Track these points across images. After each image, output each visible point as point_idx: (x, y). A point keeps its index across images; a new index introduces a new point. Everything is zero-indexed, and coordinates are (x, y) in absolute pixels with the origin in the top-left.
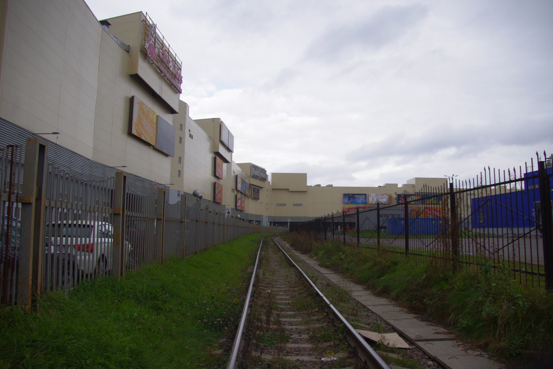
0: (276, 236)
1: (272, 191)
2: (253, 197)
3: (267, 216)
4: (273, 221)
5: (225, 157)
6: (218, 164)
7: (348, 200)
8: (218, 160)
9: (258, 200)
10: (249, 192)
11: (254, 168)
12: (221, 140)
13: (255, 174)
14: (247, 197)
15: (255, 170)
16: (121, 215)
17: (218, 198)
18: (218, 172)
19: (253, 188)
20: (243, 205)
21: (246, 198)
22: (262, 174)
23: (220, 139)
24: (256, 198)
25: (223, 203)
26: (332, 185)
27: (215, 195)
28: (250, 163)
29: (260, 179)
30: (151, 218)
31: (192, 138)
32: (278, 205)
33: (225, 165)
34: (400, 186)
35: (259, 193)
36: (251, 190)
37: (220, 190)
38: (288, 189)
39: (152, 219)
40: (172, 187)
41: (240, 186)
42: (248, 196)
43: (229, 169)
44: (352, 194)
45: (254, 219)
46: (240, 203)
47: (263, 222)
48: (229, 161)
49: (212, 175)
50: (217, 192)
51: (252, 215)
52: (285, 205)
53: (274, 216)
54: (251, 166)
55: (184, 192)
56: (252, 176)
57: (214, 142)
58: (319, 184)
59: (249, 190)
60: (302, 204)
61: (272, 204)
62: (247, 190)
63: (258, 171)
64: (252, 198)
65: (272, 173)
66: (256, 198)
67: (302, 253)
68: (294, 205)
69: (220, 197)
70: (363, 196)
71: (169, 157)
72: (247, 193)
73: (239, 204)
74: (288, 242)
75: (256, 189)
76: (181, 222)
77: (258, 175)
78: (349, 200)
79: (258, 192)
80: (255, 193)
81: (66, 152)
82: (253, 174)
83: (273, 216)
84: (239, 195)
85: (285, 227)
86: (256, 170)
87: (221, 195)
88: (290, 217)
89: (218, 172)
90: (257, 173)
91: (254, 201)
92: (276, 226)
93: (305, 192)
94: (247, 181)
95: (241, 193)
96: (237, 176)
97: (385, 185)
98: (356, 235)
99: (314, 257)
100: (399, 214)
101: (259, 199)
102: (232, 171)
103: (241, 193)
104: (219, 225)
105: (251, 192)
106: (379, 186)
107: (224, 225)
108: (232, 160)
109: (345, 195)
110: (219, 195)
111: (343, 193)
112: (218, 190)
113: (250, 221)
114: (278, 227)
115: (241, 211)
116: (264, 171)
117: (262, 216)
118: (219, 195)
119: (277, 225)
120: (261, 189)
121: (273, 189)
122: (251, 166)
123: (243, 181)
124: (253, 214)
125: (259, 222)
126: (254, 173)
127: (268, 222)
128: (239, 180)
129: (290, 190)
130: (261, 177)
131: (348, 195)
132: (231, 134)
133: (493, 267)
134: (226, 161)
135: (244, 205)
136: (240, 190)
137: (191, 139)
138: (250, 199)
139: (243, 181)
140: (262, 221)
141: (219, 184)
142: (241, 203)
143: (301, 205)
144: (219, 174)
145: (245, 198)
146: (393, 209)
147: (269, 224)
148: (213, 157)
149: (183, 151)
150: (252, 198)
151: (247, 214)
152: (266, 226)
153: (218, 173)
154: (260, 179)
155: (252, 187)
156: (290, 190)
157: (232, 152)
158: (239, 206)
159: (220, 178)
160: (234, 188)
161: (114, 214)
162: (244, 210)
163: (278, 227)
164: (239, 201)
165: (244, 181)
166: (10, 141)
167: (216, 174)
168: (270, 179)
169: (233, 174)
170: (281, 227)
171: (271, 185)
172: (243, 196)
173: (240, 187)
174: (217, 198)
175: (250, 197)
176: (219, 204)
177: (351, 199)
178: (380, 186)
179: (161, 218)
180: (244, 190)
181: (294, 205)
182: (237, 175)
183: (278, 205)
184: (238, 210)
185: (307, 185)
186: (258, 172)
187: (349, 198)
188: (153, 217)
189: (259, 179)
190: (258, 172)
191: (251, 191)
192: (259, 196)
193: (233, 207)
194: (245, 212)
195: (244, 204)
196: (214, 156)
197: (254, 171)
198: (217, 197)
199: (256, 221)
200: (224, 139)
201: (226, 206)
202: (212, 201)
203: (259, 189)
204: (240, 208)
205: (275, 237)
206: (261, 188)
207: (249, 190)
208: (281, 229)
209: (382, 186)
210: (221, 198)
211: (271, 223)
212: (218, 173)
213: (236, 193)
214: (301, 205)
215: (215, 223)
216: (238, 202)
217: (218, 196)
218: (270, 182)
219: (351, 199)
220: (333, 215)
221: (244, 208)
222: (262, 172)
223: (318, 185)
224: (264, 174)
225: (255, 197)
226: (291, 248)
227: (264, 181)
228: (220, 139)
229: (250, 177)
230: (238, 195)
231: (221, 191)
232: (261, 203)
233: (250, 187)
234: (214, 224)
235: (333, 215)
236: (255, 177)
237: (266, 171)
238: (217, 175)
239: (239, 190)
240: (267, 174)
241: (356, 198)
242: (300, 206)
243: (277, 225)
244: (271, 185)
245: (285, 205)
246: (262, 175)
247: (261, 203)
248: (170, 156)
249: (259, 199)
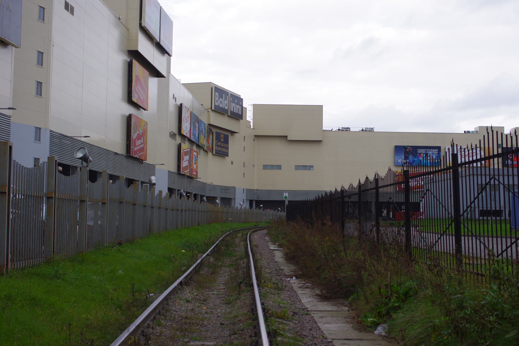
0: (256, 229)
1: (254, 140)
2: (216, 150)
3: (244, 189)
4: (255, 198)
5: (152, 63)
6: (137, 77)
7: (403, 157)
8: (138, 68)
9: (227, 158)
10: (208, 140)
11: (217, 94)
12: (143, 25)
13: (221, 106)
14: (204, 150)
15: (221, 96)
16: (7, 193)
17: (136, 149)
18: (138, 94)
19: (217, 133)
20: (195, 166)
21: (202, 152)
22: (234, 105)
23: (140, 24)
24: (222, 153)
25: (149, 160)
26: (372, 129)
27: (130, 141)
28: (210, 83)
29: (229, 114)
30: (33, 196)
31: (72, 13)
32: (265, 167)
33: (153, 82)
34: (507, 131)
35: (228, 143)
36: (211, 136)
37: (142, 133)
38: (286, 137)
39: (65, 199)
40: (16, 118)
41: (189, 126)
42: (205, 149)
43: (163, 91)
44: (411, 147)
45: (219, 195)
46: (187, 162)
47: (236, 200)
48: (163, 72)
49: (123, 100)
50: (134, 136)
51: (214, 187)
52: (279, 167)
53: (257, 190)
54: (212, 88)
55: (51, 131)
56: (213, 108)
57: (128, 30)
58: (346, 126)
59: (208, 137)
60: (312, 166)
61: (254, 166)
62: (202, 136)
63: (226, 99)
64: (214, 153)
65: (254, 105)
66: (222, 153)
67: (323, 298)
68: (297, 167)
69: (142, 146)
70: (434, 150)
71: (10, 47)
72: (203, 141)
73: (185, 164)
74: (280, 246)
75: (222, 136)
76: (133, 204)
77: (226, 108)
78: (406, 158)
79: (226, 141)
80: (219, 143)
81: (87, 145)
82: (215, 105)
83: (255, 188)
84: (185, 146)
85: (278, 210)
86: (222, 98)
87: (145, 143)
88: (289, 192)
89: (138, 94)
90: (224, 104)
91: (218, 160)
92: (259, 209)
93: (320, 141)
94: (204, 119)
95: (190, 140)
96: (180, 108)
97: (478, 130)
98: (452, 229)
99: (376, 325)
100: (511, 183)
101: (228, 156)
102: (171, 96)
103: (190, 140)
104: (145, 206)
105: (211, 142)
106: (465, 132)
107: (167, 209)
108: (169, 72)
109: (398, 149)
110: (138, 143)
111: (393, 146)
112: (137, 133)
113: (211, 199)
114: (263, 210)
115: (188, 177)
116: (238, 100)
117: (234, 188)
118: (138, 143)
119: (261, 206)
120: (232, 135)
121: (256, 136)
122: (212, 88)
123: (195, 119)
124: (214, 184)
125: (227, 201)
126: (217, 104)
127: (247, 200)
128: (185, 115)
129: (289, 138)
130: (231, 112)
131: (405, 148)
132: (166, 16)
133: (171, 196)
134: (156, 73)
135: (197, 167)
136: (188, 135)
137: (67, 14)
138: (210, 154)
139: (195, 119)
140: (234, 199)
141: (139, 120)
142: (190, 161)
143: (312, 168)
144: (139, 97)
145: (198, 154)
146: (483, 177)
147: (247, 205)
148: (126, 60)
149: (48, 39)
150: (214, 153)
151: (204, 184)
152: (239, 208)
153: (136, 96)
154: (229, 114)
155: (214, 130)
156: (289, 138)
157: (169, 55)
158: (186, 167)
159: (141, 105)
160: (175, 131)
161: (80, 201)
162: (197, 175)
163: (263, 210)
164: (186, 158)
165: (198, 118)
166: (4, 126)
167: (131, 97)
168: (249, 116)
169: (172, 102)
170: (272, 211)
171: (252, 127)
172: (195, 148)
173: (188, 130)
174: (134, 148)
175: (210, 151)
176: (140, 161)
177: (411, 158)
178: (469, 132)
179: (4, 191)
180: (197, 135)
181: (297, 167)
182: (181, 105)
183: (265, 167)
184: (184, 175)
185: (324, 129)
186: (226, 102)
187: (405, 154)
188: (62, 197)
189: (228, 116)
190: (226, 102)
191: (211, 139)
192: (228, 148)
193: (173, 168)
194: (198, 180)
195: (196, 163)
196: (129, 60)
197: (217, 99)
198: (135, 146)
199: (222, 199)
200: (153, 28)
201: (157, 167)
202: (122, 155)
203: (228, 136)
204: (187, 172)
205: (254, 232)
206: (233, 133)
207: (208, 137)
208: (270, 214)
209: (473, 132)
210: (142, 150)
211: (251, 202)
212: (136, 96)
213: (179, 139)
214: (310, 167)
215: (154, 206)
216: (183, 160)
217: (137, 144)
218: (250, 122)
219: (411, 158)
220: (455, 157)
221: (197, 172)
222: (233, 102)
223: (344, 128)
224: (238, 106)
225: (220, 151)
226: (287, 268)
227: (238, 119)
228: (140, 24)
229: (210, 110)
230: (183, 145)
231: (143, 136)
232: (232, 163)
233: (210, 132)
234: (228, 213)
235: (455, 157)
236: (219, 111)
237: (242, 100)
238: (134, 99)
239: (185, 134)
240: (244, 106)
241: (420, 154)
242: (310, 169)
243: (261, 206)
244: (252, 127)
245: (279, 167)
246: (236, 109)
247: (232, 163)
248: (13, 45)
249: (228, 156)
